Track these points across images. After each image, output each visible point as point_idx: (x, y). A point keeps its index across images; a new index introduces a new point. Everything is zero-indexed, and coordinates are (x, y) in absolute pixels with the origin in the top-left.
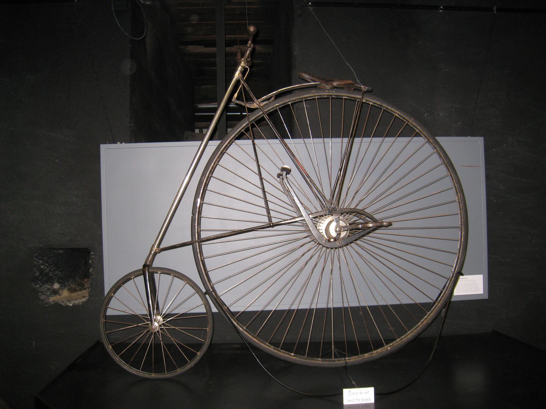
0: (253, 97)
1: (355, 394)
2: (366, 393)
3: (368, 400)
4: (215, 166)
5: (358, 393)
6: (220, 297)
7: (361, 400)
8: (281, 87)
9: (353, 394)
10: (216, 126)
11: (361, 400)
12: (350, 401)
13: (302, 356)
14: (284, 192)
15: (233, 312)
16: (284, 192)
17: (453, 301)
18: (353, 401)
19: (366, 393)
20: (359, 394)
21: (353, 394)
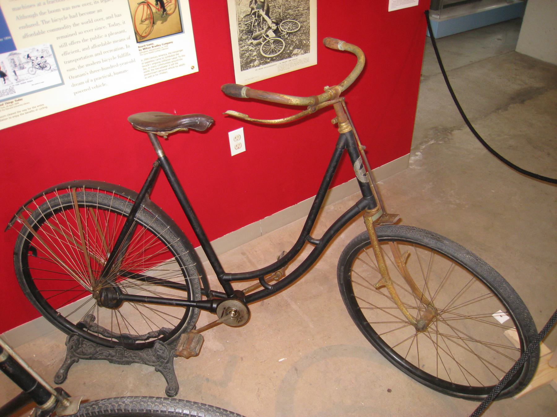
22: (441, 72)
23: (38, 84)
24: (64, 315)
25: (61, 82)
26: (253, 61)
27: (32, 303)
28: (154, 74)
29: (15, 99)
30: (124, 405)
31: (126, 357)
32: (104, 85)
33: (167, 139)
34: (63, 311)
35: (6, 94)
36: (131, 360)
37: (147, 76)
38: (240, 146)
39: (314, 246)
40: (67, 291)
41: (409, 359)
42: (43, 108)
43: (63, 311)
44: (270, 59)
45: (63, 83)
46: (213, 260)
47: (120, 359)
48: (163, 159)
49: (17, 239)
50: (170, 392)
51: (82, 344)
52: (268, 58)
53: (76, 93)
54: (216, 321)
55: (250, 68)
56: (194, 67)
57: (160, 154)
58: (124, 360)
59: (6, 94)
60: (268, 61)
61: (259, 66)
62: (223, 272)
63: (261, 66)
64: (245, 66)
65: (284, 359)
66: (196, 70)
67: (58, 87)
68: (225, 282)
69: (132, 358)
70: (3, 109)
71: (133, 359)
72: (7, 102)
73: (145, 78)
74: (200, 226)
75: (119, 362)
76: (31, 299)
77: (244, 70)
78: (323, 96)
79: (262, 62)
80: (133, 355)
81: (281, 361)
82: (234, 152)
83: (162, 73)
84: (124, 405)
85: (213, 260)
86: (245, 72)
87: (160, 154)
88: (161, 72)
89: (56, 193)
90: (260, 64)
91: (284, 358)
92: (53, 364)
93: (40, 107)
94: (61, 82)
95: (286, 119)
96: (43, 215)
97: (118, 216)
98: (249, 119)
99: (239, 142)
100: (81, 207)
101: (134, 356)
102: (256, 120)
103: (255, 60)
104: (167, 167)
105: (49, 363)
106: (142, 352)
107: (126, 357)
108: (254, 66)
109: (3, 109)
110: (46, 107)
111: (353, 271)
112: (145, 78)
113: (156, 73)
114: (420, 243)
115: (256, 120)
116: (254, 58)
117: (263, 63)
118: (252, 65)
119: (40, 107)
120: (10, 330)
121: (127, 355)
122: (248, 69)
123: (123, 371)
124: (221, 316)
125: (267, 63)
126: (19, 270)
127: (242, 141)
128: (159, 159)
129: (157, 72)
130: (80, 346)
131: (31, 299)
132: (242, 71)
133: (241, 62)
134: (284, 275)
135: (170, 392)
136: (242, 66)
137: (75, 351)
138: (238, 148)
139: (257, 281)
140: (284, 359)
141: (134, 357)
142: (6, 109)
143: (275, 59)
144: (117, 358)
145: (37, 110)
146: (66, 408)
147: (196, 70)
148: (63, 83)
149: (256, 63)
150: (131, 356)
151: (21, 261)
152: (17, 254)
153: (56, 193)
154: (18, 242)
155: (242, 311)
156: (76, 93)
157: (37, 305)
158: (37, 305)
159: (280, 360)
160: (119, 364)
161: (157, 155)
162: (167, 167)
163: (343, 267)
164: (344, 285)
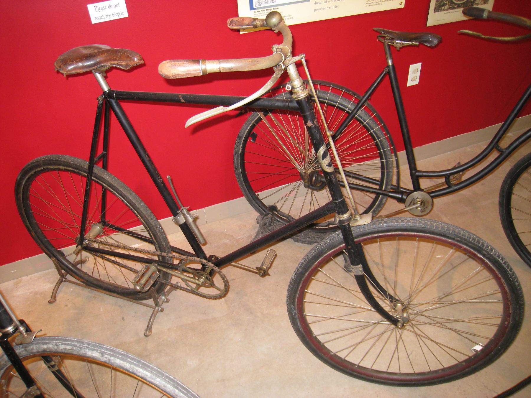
0: (53, 194)
1: (103, 9)
2: (116, 6)
3: (121, 14)
4: (391, 382)
5: (106, 7)
6: (262, 201)
7: (111, 16)
8: (515, 233)
9: (100, 9)
10: (124, 296)
11: (111, 16)
12: (99, 18)
13: (242, 179)
14: (289, 176)
15: (476, 345)
16: (289, 176)
17: (419, 63)
18: (102, 18)
19: (116, 6)
20: (107, 8)
21: (100, 9)
24: (260, 197)
26: (444, 5)
27: (239, 183)
28: (373, 4)
29: (267, 9)
30: (406, 221)
31: (309, 238)
32: (336, 7)
33: (398, 51)
34: (261, 195)
35: (269, 2)
36: (313, 240)
37: (368, 5)
38: (415, 79)
39: (499, 153)
40: (275, 174)
41: (417, 371)
42: (291, 18)
43: (261, 195)
44: (457, 5)
46: (411, 157)
47: (304, 239)
48: (391, 67)
49: (244, 125)
50: (348, 267)
51: (274, 223)
52: (456, 4)
53: (316, 10)
54: (403, 209)
55: (441, 11)
57: (390, 63)
58: (307, 240)
59: (269, 2)
60: (456, 7)
61: (447, 10)
62: (415, 169)
63: (449, 11)
64: (438, 9)
65: (440, 256)
68: (416, 178)
69: (314, 239)
71: (316, 240)
72: (268, 9)
73: (366, 6)
74: (407, 127)
75: (302, 241)
76: (240, 179)
77: (436, 12)
79: (450, 7)
80: (315, 237)
81: (438, 258)
82: (410, 83)
83: (379, 4)
84: (406, 221)
85: (411, 157)
86: (437, 14)
87: (390, 63)
88: (378, 3)
90: (449, 9)
91: (441, 255)
92: (243, 239)
93: (288, 17)
95: (516, 38)
97: (340, 111)
98: (483, 36)
99: (415, 75)
101: (318, 238)
102: (490, 37)
103: (446, 4)
104: (392, 75)
105: (239, 237)
106: (324, 235)
107: (309, 238)
108: (444, 10)
110: (292, 18)
112: (366, 6)
113: (375, 4)
115: (490, 37)
116: (446, 3)
117: (451, 8)
118: (443, 8)
119: (288, 17)
120: (210, 207)
121: (310, 237)
122: (439, 12)
123: (304, 250)
124: (408, 205)
125: (454, 8)
126: (238, 152)
127: (418, 75)
128: (388, 66)
129: (375, 2)
130: (272, 224)
131: (240, 179)
132: (434, 12)
133: (436, 5)
134: (461, 179)
135: (348, 267)
136: (435, 8)
137: (267, 228)
138: (414, 81)
139: (443, 180)
140: (440, 256)
141: (317, 239)
143: (461, 6)
144: (301, 238)
146: (357, 220)
149: (446, 7)
150: (314, 237)
151: (242, 144)
152: (240, 138)
154: (245, 127)
155: (428, 202)
156: (316, 10)
157: (243, 186)
158: (243, 186)
159: (437, 257)
160: (302, 243)
161: (387, 63)
162: (392, 75)
163: (510, 180)
164: (505, 196)
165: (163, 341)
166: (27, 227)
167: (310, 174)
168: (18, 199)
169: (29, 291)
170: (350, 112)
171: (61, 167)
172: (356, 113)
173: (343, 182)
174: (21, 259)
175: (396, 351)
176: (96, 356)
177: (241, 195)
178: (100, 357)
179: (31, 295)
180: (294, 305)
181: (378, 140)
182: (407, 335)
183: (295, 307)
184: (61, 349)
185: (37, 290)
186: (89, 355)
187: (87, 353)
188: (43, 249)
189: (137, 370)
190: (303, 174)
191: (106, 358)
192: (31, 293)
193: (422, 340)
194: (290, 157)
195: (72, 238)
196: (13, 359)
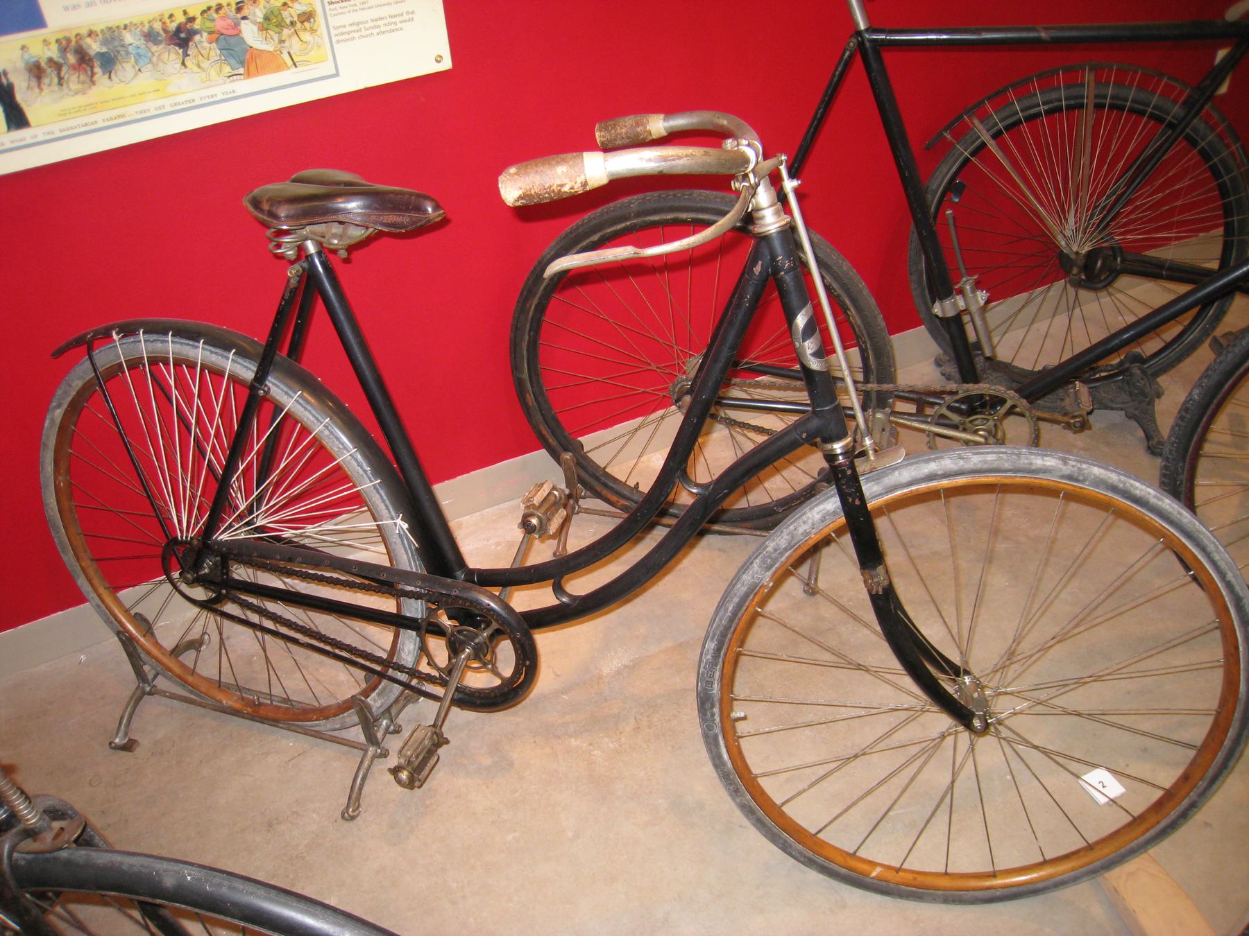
22: (1094, 341)
23: (378, 6)
25: (335, 72)
39: (547, 586)
45: (337, 75)
47: (1052, 402)
56: (441, 57)
66: (447, 64)
67: (302, 86)
70: (355, 8)
78: (611, 135)
89: (1011, 94)
94: (335, 72)
96: (1216, 160)
100: (1099, 107)
109: (355, 8)
111: (756, 776)
114: (704, 205)
142: (361, 9)
145: (349, 12)
147: (447, 64)
148: (337, 75)
153: (1011, 94)
165: (850, 600)
166: (520, 383)
167: (1084, 256)
168: (523, 310)
169: (491, 542)
170: (1175, 122)
171: (684, 216)
172: (1187, 125)
173: (851, 409)
174: (468, 472)
175: (948, 799)
176: (1052, 466)
177: (917, 323)
178: (1061, 466)
179: (499, 548)
180: (1184, 461)
181: (1226, 178)
182: (987, 744)
183: (1184, 466)
184: (974, 464)
185: (509, 538)
186: (1038, 466)
187: (1034, 461)
188: (541, 436)
189: (1132, 485)
190: (1073, 256)
191: (1073, 466)
192: (498, 544)
193: (938, 806)
194: (1047, 223)
195: (647, 390)
196: (846, 508)
